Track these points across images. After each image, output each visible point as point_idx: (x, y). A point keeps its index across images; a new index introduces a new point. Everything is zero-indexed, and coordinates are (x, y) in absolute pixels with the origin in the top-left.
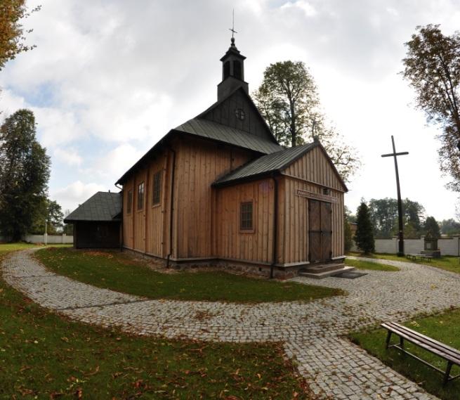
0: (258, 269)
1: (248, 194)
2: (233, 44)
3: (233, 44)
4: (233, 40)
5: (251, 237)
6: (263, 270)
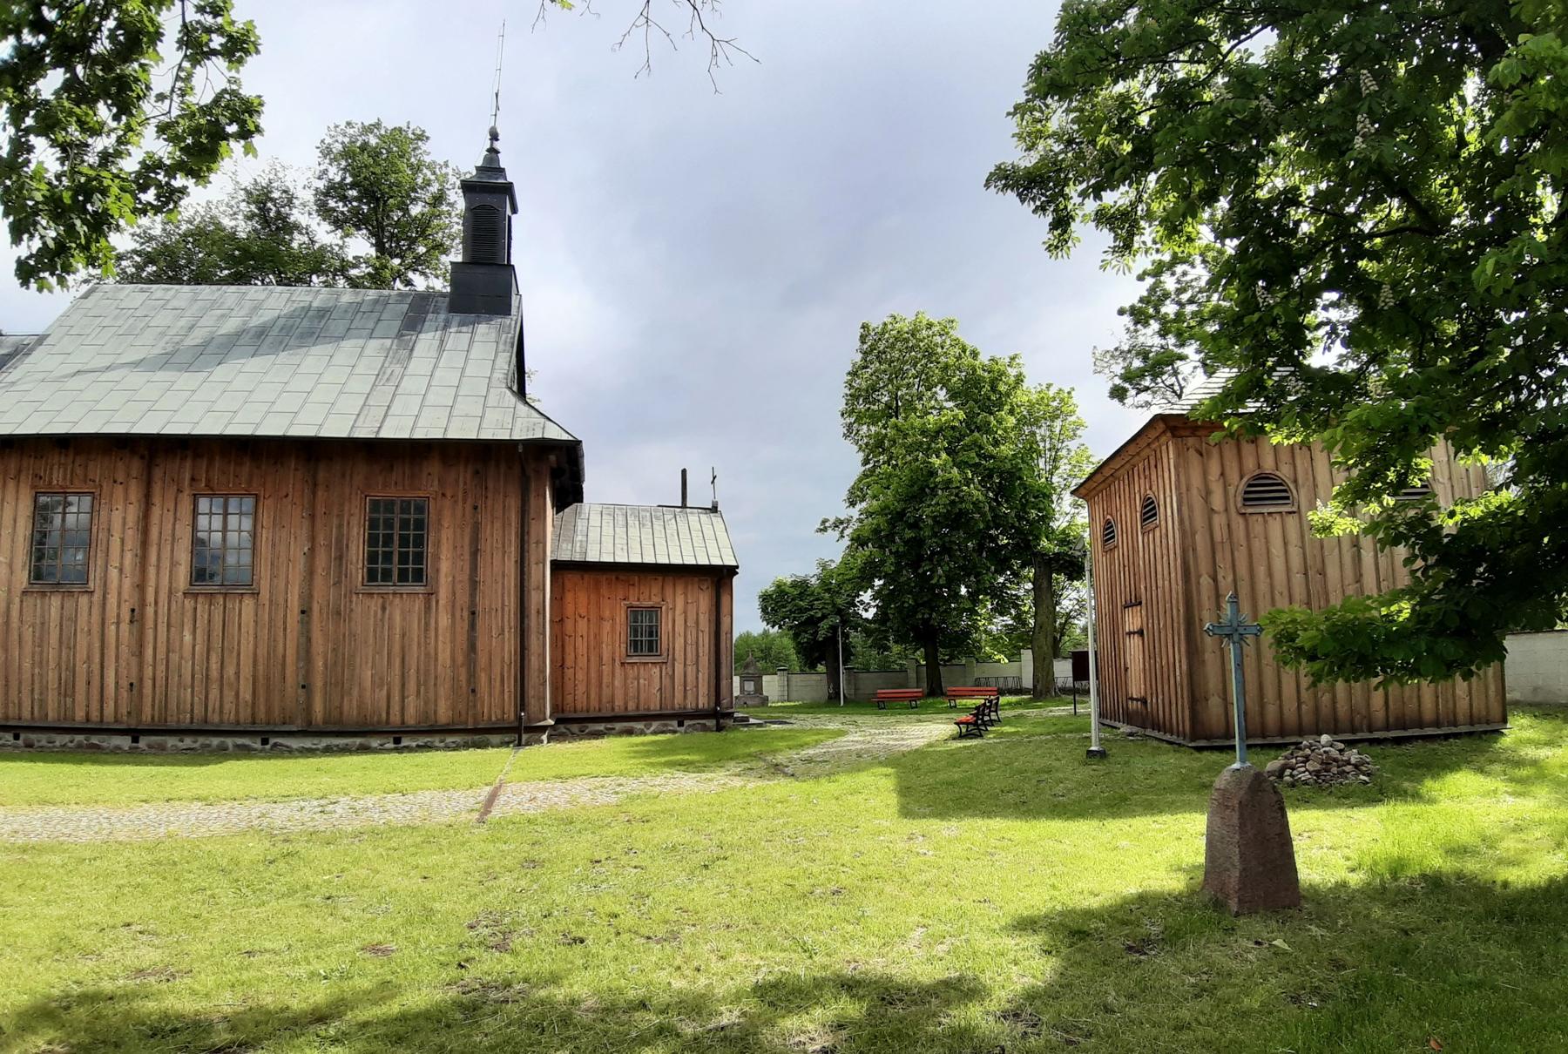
0: (675, 723)
1: (648, 595)
2: (493, 151)
3: (493, 151)
4: (494, 136)
5: (656, 670)
6: (687, 723)
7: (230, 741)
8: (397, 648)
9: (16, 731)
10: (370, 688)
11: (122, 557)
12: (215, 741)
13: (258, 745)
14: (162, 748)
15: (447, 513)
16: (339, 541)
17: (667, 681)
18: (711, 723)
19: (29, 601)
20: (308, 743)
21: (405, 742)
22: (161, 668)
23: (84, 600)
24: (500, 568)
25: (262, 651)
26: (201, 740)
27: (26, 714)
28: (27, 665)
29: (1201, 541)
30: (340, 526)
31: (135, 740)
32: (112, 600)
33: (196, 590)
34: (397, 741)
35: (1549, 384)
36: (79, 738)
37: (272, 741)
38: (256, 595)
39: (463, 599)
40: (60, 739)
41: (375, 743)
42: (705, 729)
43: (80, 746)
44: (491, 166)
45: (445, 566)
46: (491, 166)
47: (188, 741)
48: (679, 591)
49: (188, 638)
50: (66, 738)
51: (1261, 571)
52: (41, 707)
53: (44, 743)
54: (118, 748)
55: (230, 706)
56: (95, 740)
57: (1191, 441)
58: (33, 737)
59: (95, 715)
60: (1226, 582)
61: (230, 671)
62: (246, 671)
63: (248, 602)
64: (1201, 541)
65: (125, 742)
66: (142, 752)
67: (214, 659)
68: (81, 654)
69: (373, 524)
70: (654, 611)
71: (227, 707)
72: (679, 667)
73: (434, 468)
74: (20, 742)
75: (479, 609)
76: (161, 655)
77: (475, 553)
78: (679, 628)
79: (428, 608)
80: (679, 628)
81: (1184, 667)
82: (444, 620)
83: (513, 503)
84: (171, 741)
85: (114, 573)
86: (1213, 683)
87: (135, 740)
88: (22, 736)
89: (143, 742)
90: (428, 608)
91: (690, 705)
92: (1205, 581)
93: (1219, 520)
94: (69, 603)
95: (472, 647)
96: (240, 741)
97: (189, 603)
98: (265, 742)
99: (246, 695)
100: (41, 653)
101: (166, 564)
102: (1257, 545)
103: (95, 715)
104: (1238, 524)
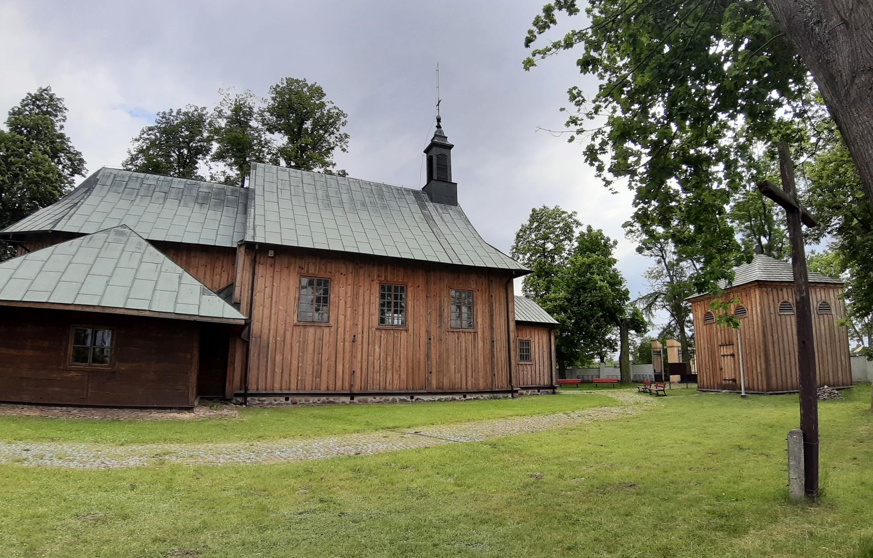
2: (439, 127)
4: (439, 120)
5: (529, 367)
7: (397, 398)
8: (463, 356)
9: (287, 396)
10: (454, 375)
11: (346, 310)
12: (391, 398)
13: (409, 399)
14: (366, 402)
15: (479, 298)
16: (440, 308)
17: (533, 372)
18: (550, 391)
19: (297, 330)
20: (430, 398)
21: (468, 397)
22: (365, 364)
23: (326, 330)
24: (500, 322)
25: (410, 355)
26: (384, 397)
27: (293, 386)
28: (295, 363)
29: (768, 322)
30: (440, 301)
31: (352, 399)
32: (341, 330)
33: (381, 327)
34: (465, 397)
35: (276, 163)
36: (323, 398)
37: (416, 397)
38: (407, 331)
39: (487, 334)
40: (312, 399)
41: (457, 397)
42: (548, 393)
43: (324, 402)
44: (439, 135)
45: (480, 320)
46: (439, 135)
47: (378, 398)
48: (536, 333)
49: (377, 349)
50: (316, 399)
51: (785, 334)
52: (302, 384)
53: (303, 402)
54: (344, 402)
55: (395, 382)
56: (331, 399)
57: (764, 289)
58: (297, 399)
59: (331, 387)
60: (776, 337)
61: (396, 365)
62: (403, 365)
63: (404, 334)
64: (768, 322)
65: (347, 399)
66: (355, 403)
67: (389, 359)
68: (325, 357)
69: (382, 296)
70: (528, 343)
71: (395, 382)
72: (537, 366)
73: (473, 277)
74: (289, 402)
75: (495, 340)
76: (365, 357)
77: (491, 316)
78: (537, 350)
79: (475, 339)
80: (537, 350)
81: (763, 366)
82: (480, 344)
83: (503, 295)
84: (370, 399)
85: (341, 318)
86: (773, 372)
87: (352, 399)
88: (290, 399)
89: (356, 399)
90: (475, 339)
91: (542, 384)
92: (770, 337)
93: (773, 316)
94: (319, 331)
95: (493, 356)
96: (402, 397)
97: (378, 333)
98: (412, 398)
99: (404, 377)
100: (303, 356)
101: (366, 314)
102: (784, 325)
103: (331, 387)
104: (778, 317)
